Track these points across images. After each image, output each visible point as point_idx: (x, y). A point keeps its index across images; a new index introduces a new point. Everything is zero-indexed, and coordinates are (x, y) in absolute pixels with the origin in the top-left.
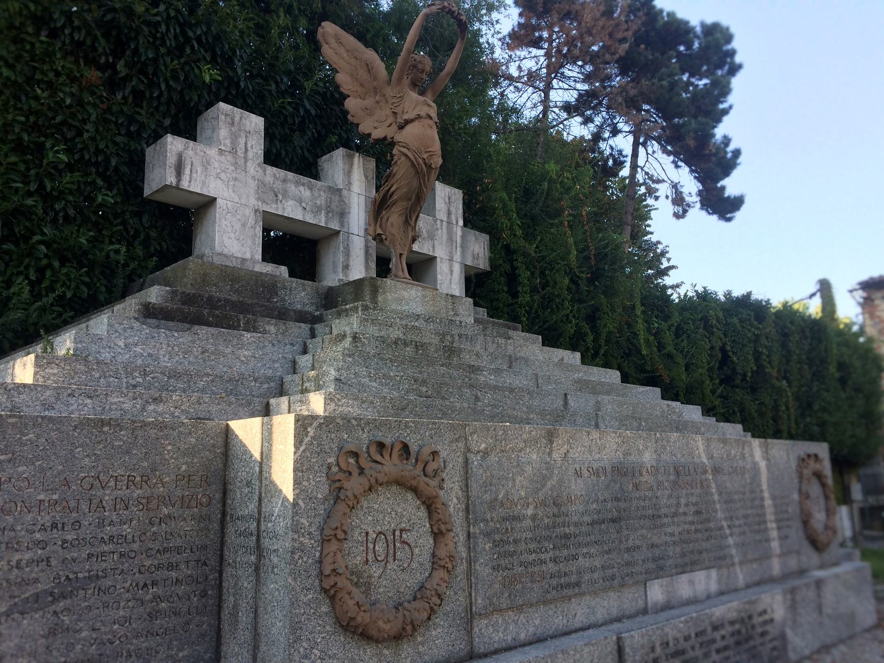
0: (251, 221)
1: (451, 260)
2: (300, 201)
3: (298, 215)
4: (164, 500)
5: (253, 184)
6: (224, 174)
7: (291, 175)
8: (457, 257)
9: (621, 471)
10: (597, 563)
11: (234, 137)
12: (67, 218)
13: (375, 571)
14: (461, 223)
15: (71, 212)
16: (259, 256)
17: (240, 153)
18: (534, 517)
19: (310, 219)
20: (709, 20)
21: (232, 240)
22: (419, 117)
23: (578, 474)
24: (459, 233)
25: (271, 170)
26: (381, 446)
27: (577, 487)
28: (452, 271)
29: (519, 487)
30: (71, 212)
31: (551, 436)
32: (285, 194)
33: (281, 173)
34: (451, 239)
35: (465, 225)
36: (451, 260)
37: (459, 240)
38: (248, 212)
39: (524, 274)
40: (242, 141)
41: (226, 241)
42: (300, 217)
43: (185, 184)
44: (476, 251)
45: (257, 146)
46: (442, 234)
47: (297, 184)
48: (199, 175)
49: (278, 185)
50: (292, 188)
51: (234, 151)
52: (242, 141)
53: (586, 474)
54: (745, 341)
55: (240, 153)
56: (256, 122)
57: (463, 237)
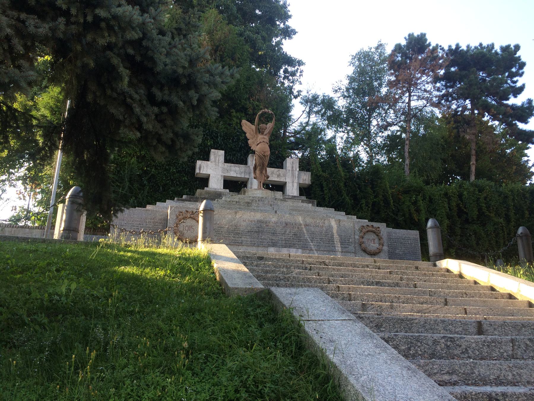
0: (220, 179)
1: (293, 182)
2: (235, 171)
3: (235, 175)
4: (157, 222)
5: (220, 169)
6: (214, 168)
7: (232, 165)
8: (296, 180)
9: (259, 221)
10: (249, 240)
11: (215, 158)
12: (177, 185)
13: (185, 232)
14: (298, 169)
15: (178, 183)
16: (222, 188)
17: (217, 161)
18: (228, 228)
19: (239, 176)
20: (504, 44)
21: (216, 184)
22: (260, 142)
23: (244, 221)
24: (297, 173)
25: (226, 164)
26: (187, 211)
27: (244, 224)
28: (293, 186)
29: (224, 221)
30: (178, 183)
31: (236, 213)
32: (231, 170)
33: (229, 165)
34: (293, 175)
35: (299, 170)
36: (293, 182)
37: (297, 176)
38: (219, 177)
39: (324, 184)
40: (218, 158)
41: (213, 185)
43: (201, 172)
44: (305, 178)
45: (222, 159)
46: (289, 174)
47: (235, 167)
48: (205, 169)
49: (228, 168)
50: (233, 168)
51: (215, 161)
52: (218, 158)
54: (471, 202)
55: (217, 161)
56: (222, 152)
57: (298, 174)
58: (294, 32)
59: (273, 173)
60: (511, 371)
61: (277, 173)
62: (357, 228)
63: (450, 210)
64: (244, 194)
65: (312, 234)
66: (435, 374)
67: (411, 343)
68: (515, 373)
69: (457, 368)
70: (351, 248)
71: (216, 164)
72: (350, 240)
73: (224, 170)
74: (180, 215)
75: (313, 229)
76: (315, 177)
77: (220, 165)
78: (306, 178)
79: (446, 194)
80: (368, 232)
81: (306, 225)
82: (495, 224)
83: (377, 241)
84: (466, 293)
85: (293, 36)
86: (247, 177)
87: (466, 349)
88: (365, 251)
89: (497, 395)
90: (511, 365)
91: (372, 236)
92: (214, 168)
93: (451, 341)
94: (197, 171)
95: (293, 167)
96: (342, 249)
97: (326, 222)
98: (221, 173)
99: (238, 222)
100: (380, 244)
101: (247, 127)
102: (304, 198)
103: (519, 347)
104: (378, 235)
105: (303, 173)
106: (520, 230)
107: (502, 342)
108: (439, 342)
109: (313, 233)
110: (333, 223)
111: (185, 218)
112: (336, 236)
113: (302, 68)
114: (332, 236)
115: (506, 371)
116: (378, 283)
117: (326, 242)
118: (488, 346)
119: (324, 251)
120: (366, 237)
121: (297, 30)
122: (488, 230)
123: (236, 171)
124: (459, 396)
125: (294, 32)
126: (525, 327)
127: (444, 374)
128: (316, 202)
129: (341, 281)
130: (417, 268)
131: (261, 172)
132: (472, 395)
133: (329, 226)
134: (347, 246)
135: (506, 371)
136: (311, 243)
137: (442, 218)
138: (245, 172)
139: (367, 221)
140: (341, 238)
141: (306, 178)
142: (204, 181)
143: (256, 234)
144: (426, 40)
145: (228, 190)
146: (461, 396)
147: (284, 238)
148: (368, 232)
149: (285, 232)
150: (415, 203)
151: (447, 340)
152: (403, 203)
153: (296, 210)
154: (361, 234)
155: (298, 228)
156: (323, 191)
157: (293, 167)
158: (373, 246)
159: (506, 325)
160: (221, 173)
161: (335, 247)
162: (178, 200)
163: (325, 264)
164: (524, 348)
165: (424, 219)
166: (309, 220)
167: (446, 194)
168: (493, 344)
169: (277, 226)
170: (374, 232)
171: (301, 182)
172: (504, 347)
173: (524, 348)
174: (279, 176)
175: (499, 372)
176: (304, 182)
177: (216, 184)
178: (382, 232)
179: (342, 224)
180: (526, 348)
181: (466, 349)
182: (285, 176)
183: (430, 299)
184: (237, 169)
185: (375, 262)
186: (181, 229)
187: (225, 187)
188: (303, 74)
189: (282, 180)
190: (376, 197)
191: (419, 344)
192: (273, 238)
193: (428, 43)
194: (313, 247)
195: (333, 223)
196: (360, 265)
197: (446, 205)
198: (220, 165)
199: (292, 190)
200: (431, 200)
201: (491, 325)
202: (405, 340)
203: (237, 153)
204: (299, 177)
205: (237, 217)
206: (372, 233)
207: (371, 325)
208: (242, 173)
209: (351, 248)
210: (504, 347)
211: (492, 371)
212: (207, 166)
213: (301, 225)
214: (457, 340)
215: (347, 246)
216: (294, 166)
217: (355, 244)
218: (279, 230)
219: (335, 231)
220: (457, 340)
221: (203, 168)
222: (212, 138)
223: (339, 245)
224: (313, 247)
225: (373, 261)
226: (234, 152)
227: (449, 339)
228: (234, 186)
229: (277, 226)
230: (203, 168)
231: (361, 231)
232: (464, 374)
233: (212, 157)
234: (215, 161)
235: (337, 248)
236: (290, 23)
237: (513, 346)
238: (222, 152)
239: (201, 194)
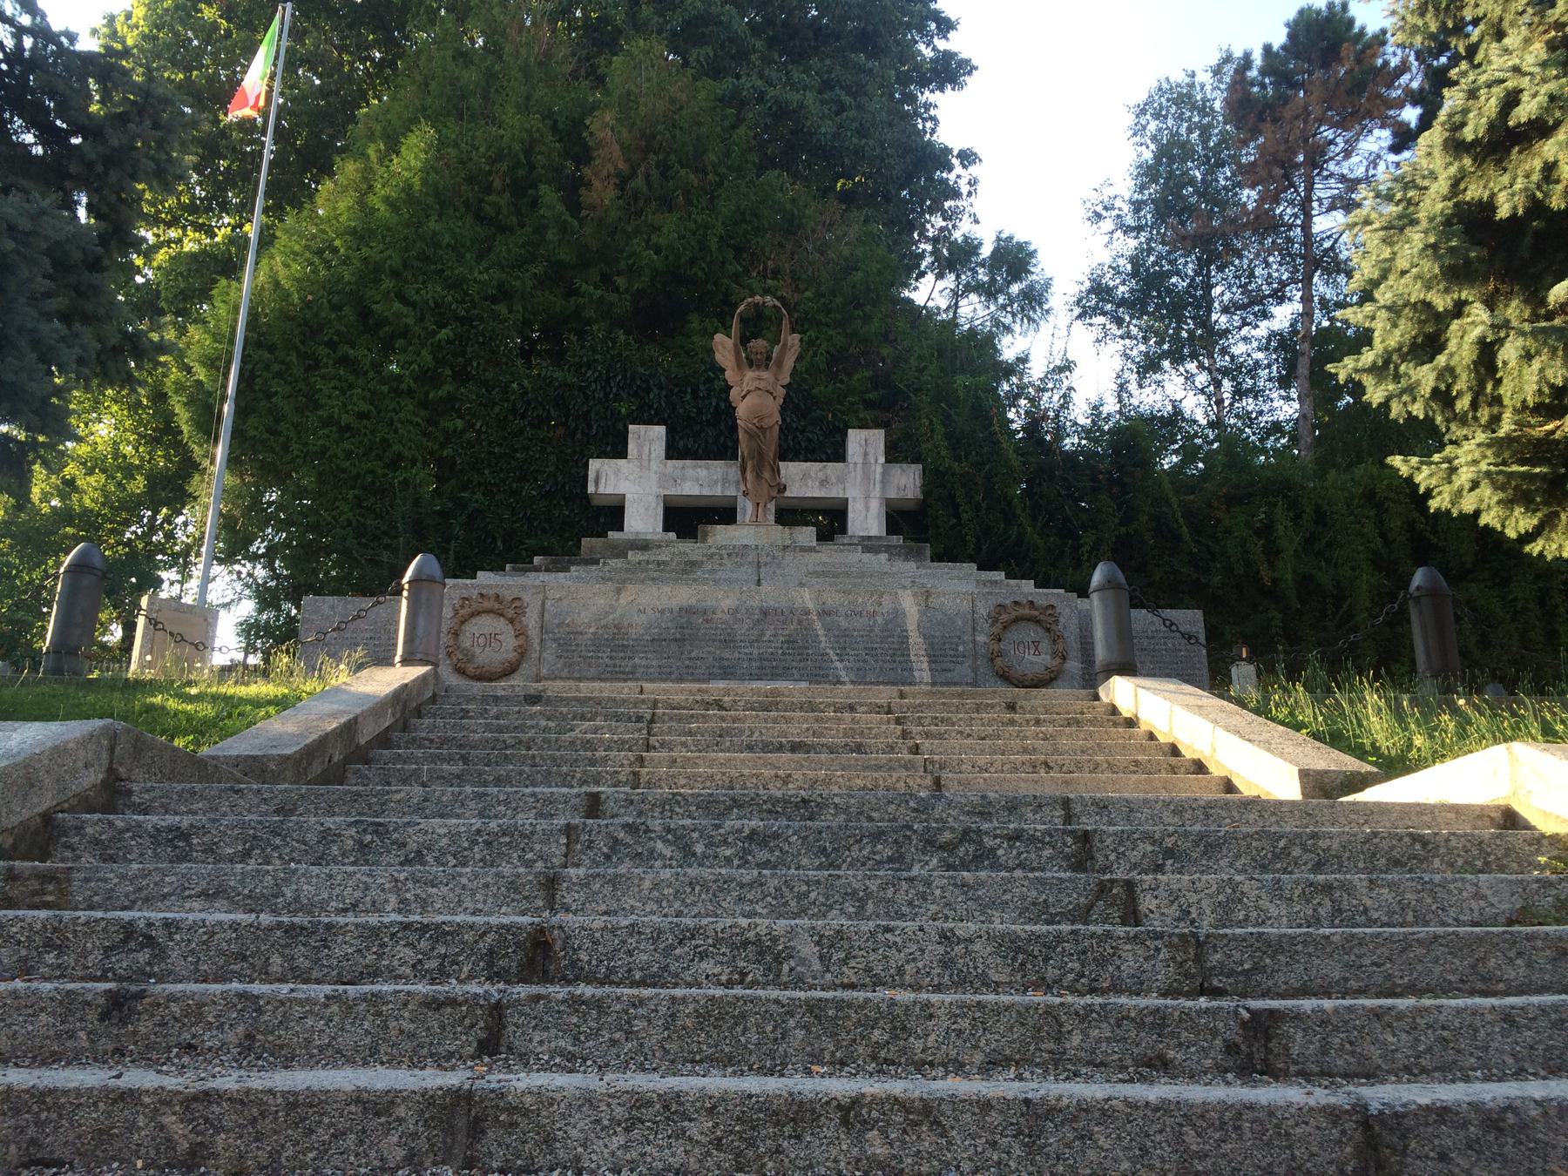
1: (867, 497)
2: (697, 480)
3: (696, 491)
5: (654, 478)
6: (639, 477)
7: (688, 462)
8: (877, 492)
9: (688, 611)
11: (640, 447)
12: (544, 531)
13: (478, 650)
14: (882, 460)
18: (594, 634)
19: (706, 492)
21: (643, 520)
24: (879, 469)
25: (669, 462)
26: (482, 595)
27: (641, 620)
28: (867, 509)
31: (618, 591)
32: (684, 479)
34: (867, 476)
35: (887, 461)
36: (867, 497)
37: (878, 477)
42: (697, 493)
43: (601, 490)
44: (903, 482)
45: (659, 448)
47: (695, 467)
49: (678, 472)
50: (690, 472)
51: (640, 455)
53: (649, 611)
56: (659, 431)
57: (884, 474)
58: (967, 67)
59: (805, 476)
60: (397, 891)
61: (820, 475)
62: (983, 610)
63: (1388, 543)
64: (704, 540)
65: (843, 640)
66: (165, 896)
67: (255, 837)
68: (408, 896)
69: (232, 884)
70: (964, 670)
71: (641, 467)
72: (961, 648)
73: (663, 478)
74: (462, 607)
75: (844, 623)
76: (934, 480)
77: (654, 466)
78: (908, 482)
79: (1370, 495)
80: (1016, 620)
81: (824, 613)
82: (1538, 577)
83: (1045, 645)
84: (1046, 764)
85: (967, 78)
86: (731, 492)
87: (419, 853)
88: (1006, 677)
89: (150, 925)
90: (402, 876)
91: (1031, 632)
92: (639, 477)
93: (376, 832)
94: (591, 489)
95: (866, 455)
96: (933, 677)
97: (886, 600)
98: (655, 490)
99: (622, 616)
100: (1054, 654)
101: (724, 347)
102: (897, 540)
103: (589, 847)
104: (1048, 630)
105: (896, 469)
106: (1419, 578)
107: (532, 833)
108: (339, 835)
109: (845, 634)
110: (909, 605)
111: (476, 614)
112: (915, 639)
113: (974, 170)
114: (904, 639)
115: (383, 890)
116: (795, 747)
117: (883, 656)
118: (488, 844)
119: (878, 683)
120: (1015, 634)
121: (974, 62)
122: (1515, 599)
123: (702, 480)
124: (39, 926)
125: (967, 67)
126: (740, 807)
127: (190, 897)
128: (928, 550)
129: (684, 744)
130: (1011, 707)
131: (758, 477)
132: (76, 924)
133: (896, 611)
134: (951, 666)
135: (383, 890)
136: (838, 664)
137: (1353, 569)
138: (725, 481)
139: (1062, 591)
140: (931, 644)
141: (908, 482)
142: (614, 514)
143: (674, 646)
144: (1351, 22)
145: (672, 535)
146: (44, 926)
147: (756, 652)
148: (1016, 620)
149: (763, 635)
150: (1265, 531)
151: (365, 830)
152: (1228, 531)
153: (824, 574)
154: (994, 630)
155: (800, 622)
156: (957, 516)
157: (866, 455)
158: (1037, 660)
159: (678, 802)
160: (655, 490)
161: (911, 669)
162: (514, 569)
163: (721, 708)
164: (605, 850)
165: (1289, 576)
166: (832, 599)
167: (1370, 495)
168: (507, 839)
169: (737, 620)
170: (1037, 621)
171: (893, 495)
172: (537, 847)
173: (605, 850)
174: (824, 482)
175: (358, 894)
176: (901, 495)
177: (643, 520)
178: (1062, 620)
179: (935, 601)
180: (611, 848)
181: (419, 853)
182: (842, 480)
183: (885, 780)
184: (703, 473)
185: (902, 696)
186: (466, 643)
187: (666, 529)
188: (979, 187)
189: (834, 492)
190: (1125, 521)
191: (278, 841)
192: (726, 655)
193: (1356, 30)
194: (843, 673)
195: (909, 605)
196: (828, 705)
197: (1369, 528)
198: (654, 466)
199: (866, 519)
200: (1321, 517)
201: (632, 802)
202: (236, 832)
203: (702, 430)
204: (884, 482)
205: (623, 601)
206: (1031, 626)
207: (264, 808)
208: (716, 483)
209: (964, 670)
210: (537, 847)
211: (337, 890)
212: (617, 472)
213: (807, 613)
214: (395, 830)
215: (951, 666)
216: (871, 450)
217: (975, 658)
218: (741, 630)
219: (912, 623)
220: (395, 830)
221: (608, 478)
222: (636, 394)
223: (925, 666)
224: (843, 673)
225: (896, 694)
226: (698, 427)
227: (370, 829)
228: (685, 518)
229: (737, 620)
230: (608, 478)
231: (996, 620)
232: (250, 897)
233: (631, 447)
234: (640, 455)
235: (916, 674)
236: (954, 43)
237: (567, 845)
238: (659, 431)
239: (591, 549)
